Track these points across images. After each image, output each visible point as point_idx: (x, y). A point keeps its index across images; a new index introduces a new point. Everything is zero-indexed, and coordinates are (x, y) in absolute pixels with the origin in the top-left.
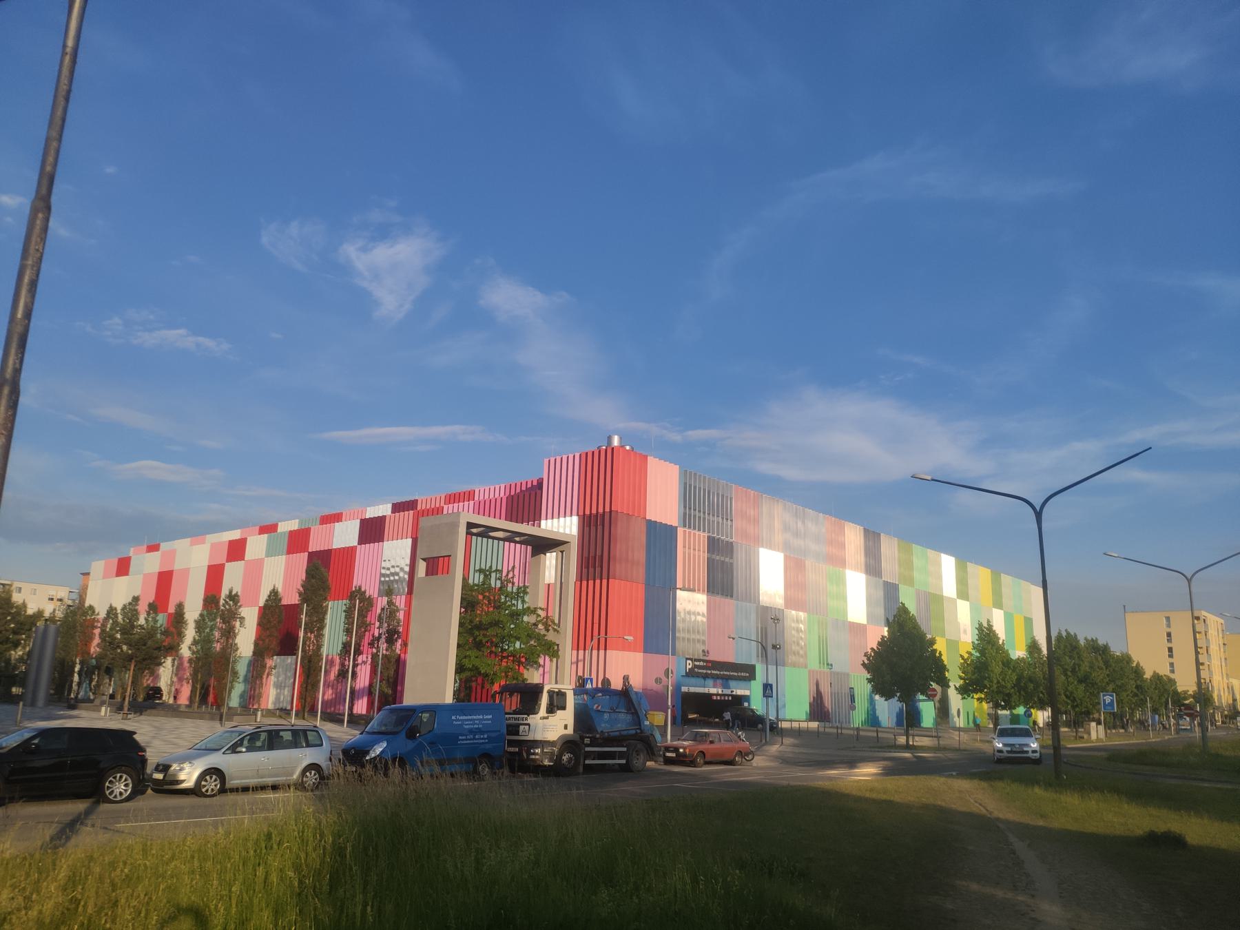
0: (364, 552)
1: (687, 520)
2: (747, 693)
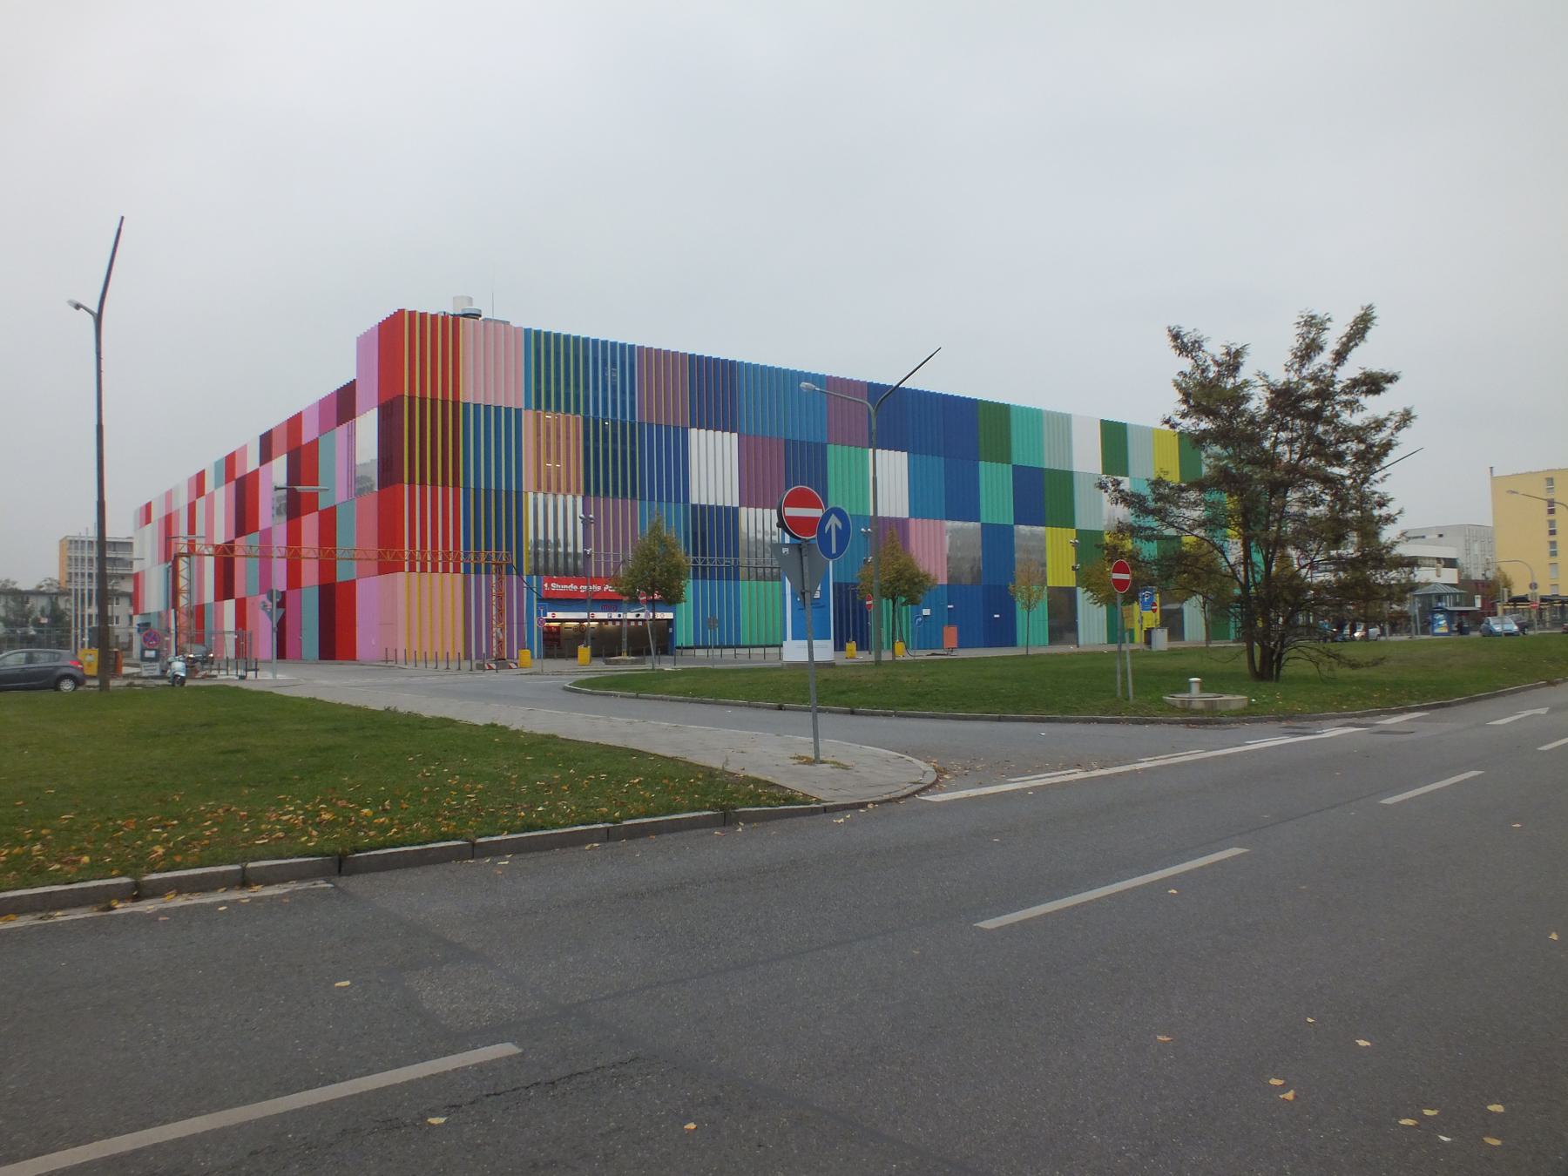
0: (263, 470)
1: (541, 398)
2: (669, 616)
